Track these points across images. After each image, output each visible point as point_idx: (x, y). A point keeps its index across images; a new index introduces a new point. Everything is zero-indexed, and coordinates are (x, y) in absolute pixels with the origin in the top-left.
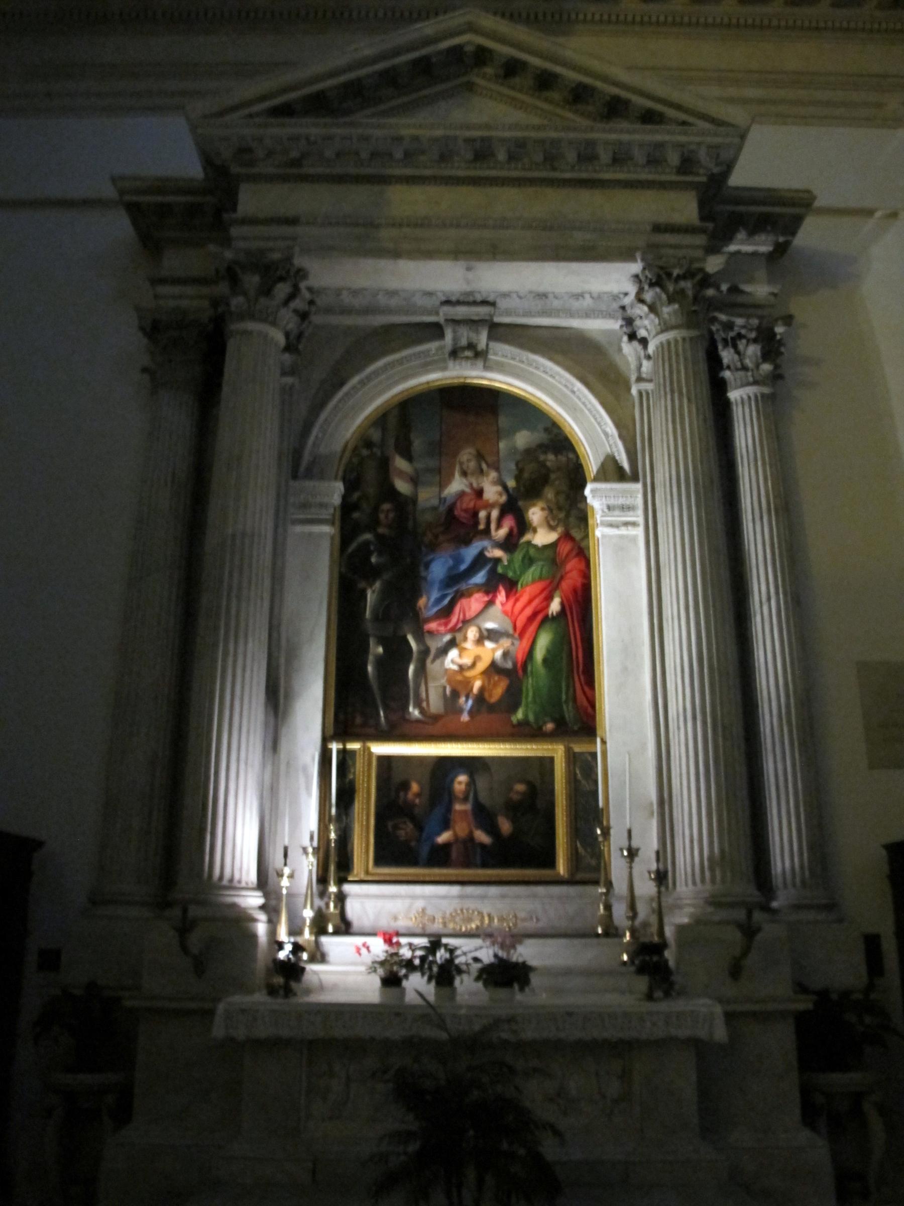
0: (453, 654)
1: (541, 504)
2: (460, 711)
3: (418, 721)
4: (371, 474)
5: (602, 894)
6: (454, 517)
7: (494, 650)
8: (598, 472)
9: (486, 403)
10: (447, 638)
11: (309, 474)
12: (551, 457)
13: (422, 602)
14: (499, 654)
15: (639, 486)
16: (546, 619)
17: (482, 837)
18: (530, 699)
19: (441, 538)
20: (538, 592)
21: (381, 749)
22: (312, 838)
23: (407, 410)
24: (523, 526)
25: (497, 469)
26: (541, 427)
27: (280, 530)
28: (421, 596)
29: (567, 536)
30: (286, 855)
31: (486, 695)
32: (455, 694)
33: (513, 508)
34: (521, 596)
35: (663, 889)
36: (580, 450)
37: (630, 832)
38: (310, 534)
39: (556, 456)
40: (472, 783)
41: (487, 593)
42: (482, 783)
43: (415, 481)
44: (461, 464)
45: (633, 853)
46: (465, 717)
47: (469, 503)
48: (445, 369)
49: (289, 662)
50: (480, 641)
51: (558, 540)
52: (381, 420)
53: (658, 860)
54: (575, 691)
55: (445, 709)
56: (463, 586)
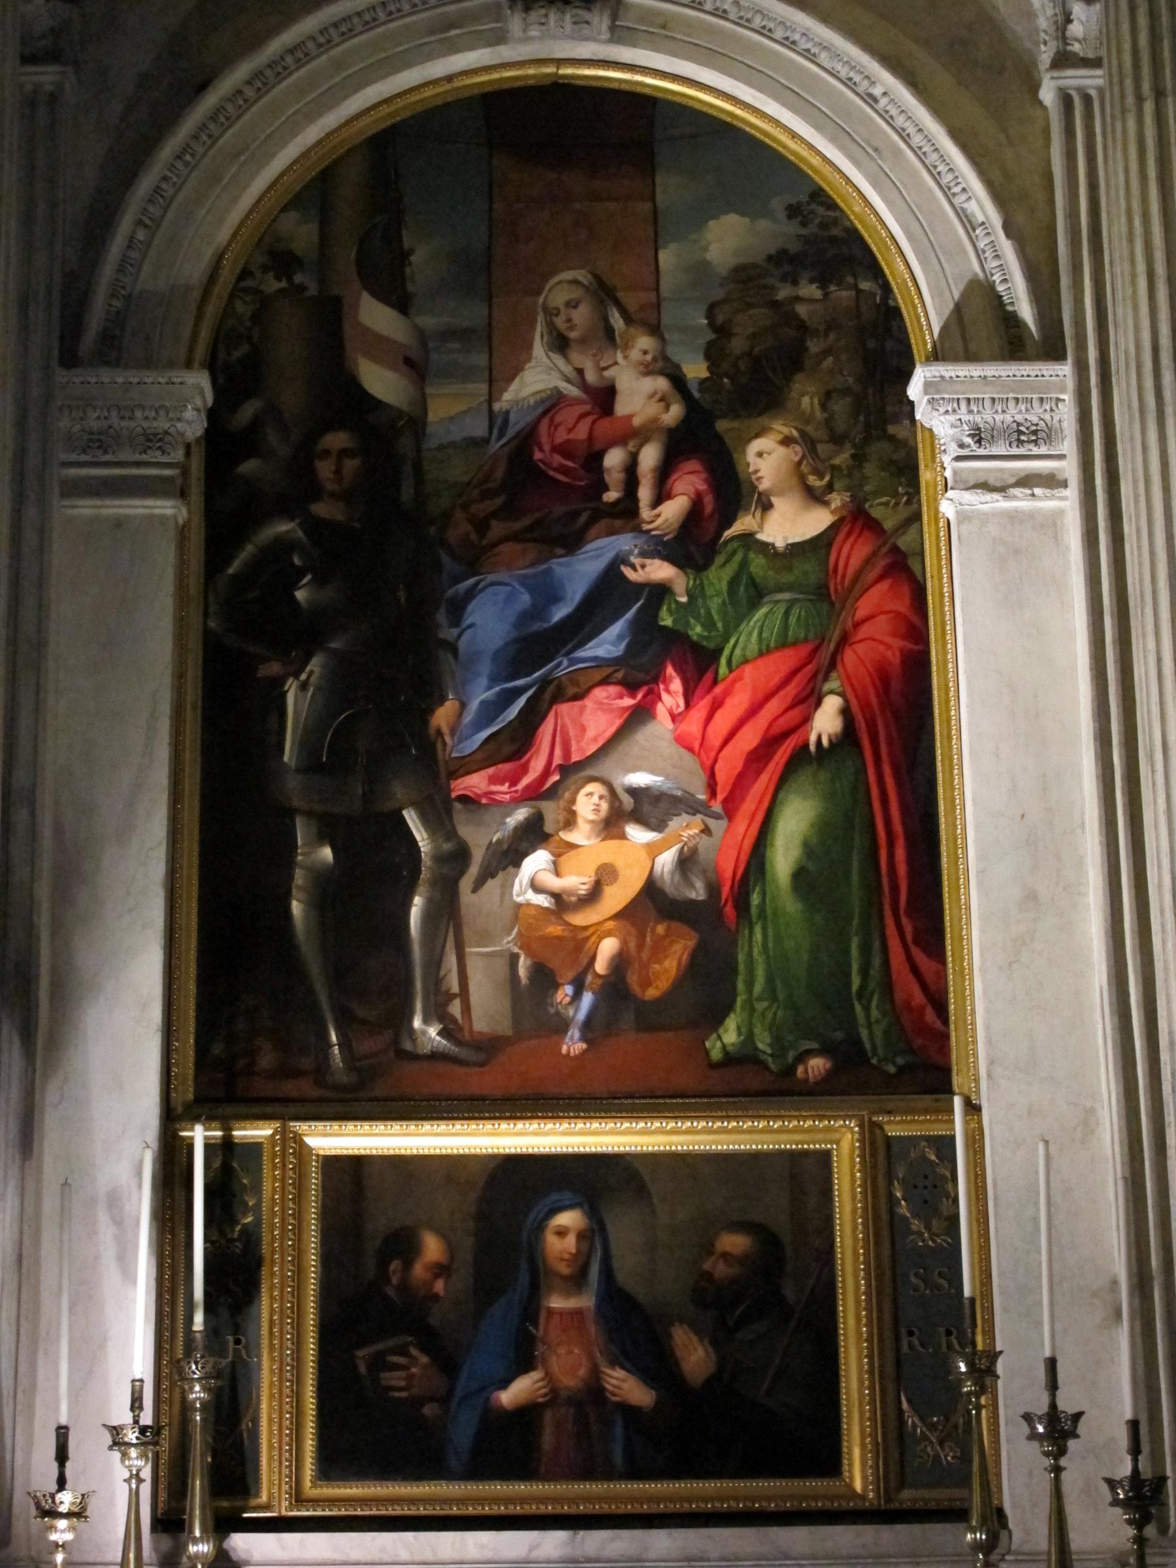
0: (537, 862)
1: (781, 428)
2: (561, 1026)
3: (436, 1056)
4: (289, 348)
5: (977, 1546)
6: (536, 474)
7: (653, 850)
8: (944, 329)
9: (622, 136)
10: (521, 814)
11: (111, 351)
12: (810, 290)
13: (442, 716)
14: (666, 860)
15: (1065, 370)
16: (801, 756)
17: (627, 1387)
18: (758, 988)
19: (497, 529)
20: (776, 680)
21: (331, 1139)
22: (136, 1403)
23: (394, 152)
24: (731, 492)
25: (655, 330)
26: (778, 205)
27: (31, 512)
28: (442, 700)
29: (857, 519)
30: (62, 1456)
31: (633, 980)
32: (544, 978)
33: (701, 440)
34: (727, 693)
35: (1150, 1531)
36: (894, 270)
37: (1052, 1364)
38: (119, 523)
39: (823, 286)
40: (595, 1233)
41: (631, 687)
42: (625, 1230)
43: (416, 367)
44: (551, 313)
45: (1059, 1430)
46: (573, 1044)
47: (575, 428)
48: (499, 38)
49: (63, 894)
50: (611, 825)
51: (834, 528)
52: (316, 189)
53: (1135, 1450)
54: (886, 963)
55: (517, 1020)
56: (562, 667)
